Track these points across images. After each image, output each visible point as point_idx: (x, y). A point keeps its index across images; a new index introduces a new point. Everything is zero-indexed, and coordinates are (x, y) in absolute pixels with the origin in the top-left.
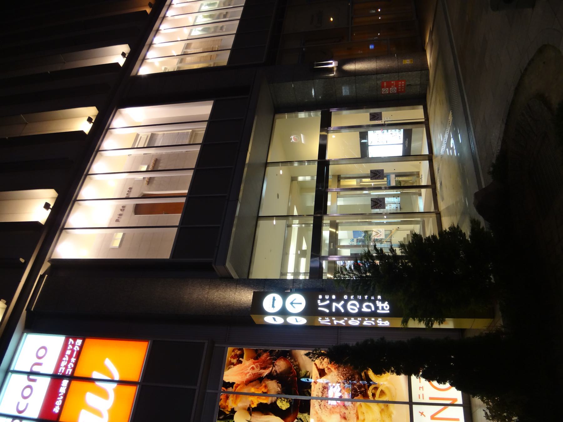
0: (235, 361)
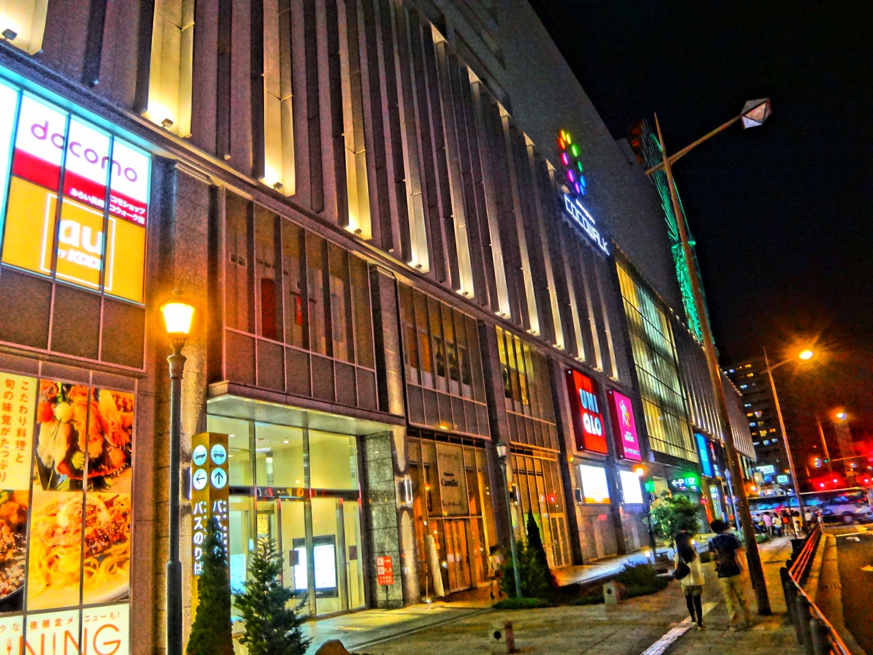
0: (120, 402)
